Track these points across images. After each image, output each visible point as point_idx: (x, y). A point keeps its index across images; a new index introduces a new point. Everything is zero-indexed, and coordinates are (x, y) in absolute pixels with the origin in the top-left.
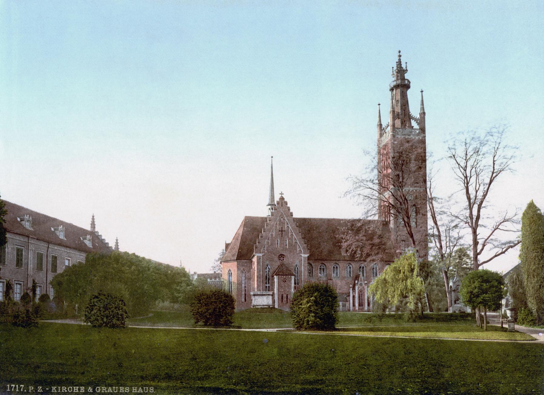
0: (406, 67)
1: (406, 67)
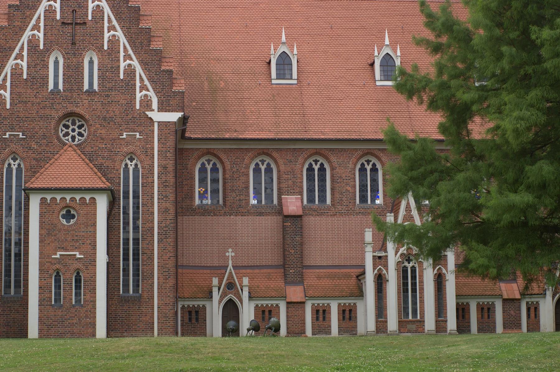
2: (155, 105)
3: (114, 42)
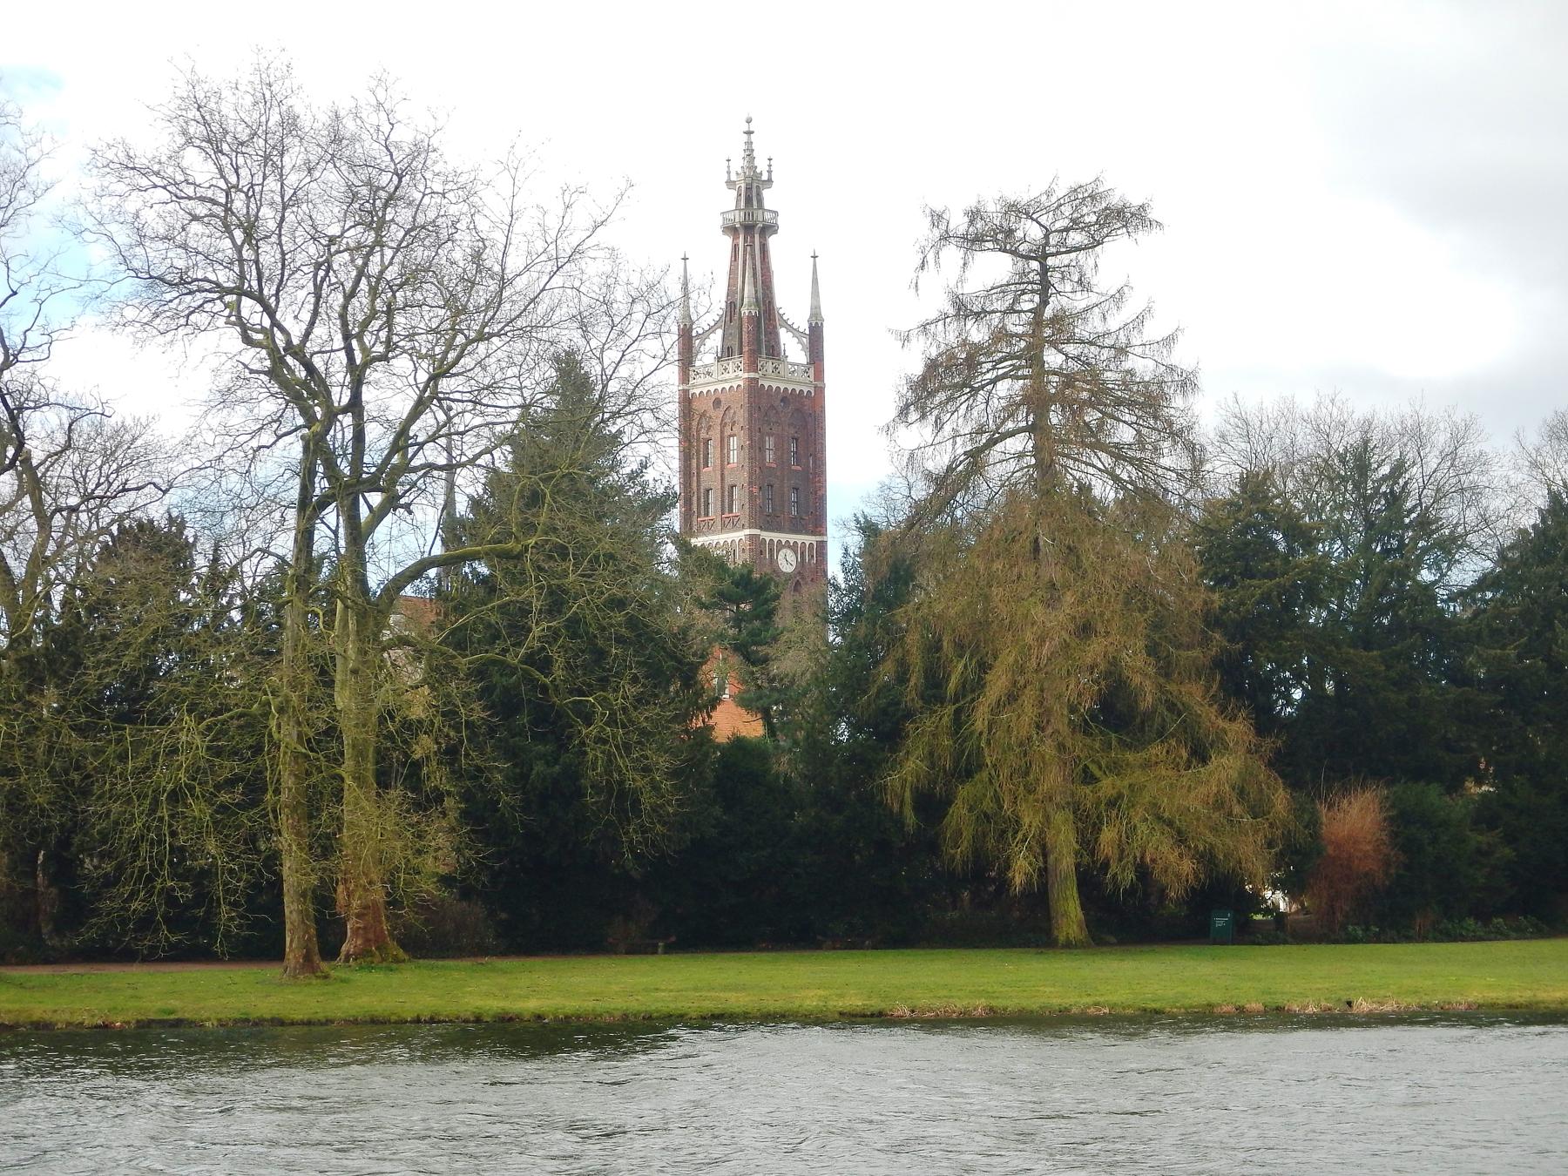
0: (770, 172)
1: (770, 172)
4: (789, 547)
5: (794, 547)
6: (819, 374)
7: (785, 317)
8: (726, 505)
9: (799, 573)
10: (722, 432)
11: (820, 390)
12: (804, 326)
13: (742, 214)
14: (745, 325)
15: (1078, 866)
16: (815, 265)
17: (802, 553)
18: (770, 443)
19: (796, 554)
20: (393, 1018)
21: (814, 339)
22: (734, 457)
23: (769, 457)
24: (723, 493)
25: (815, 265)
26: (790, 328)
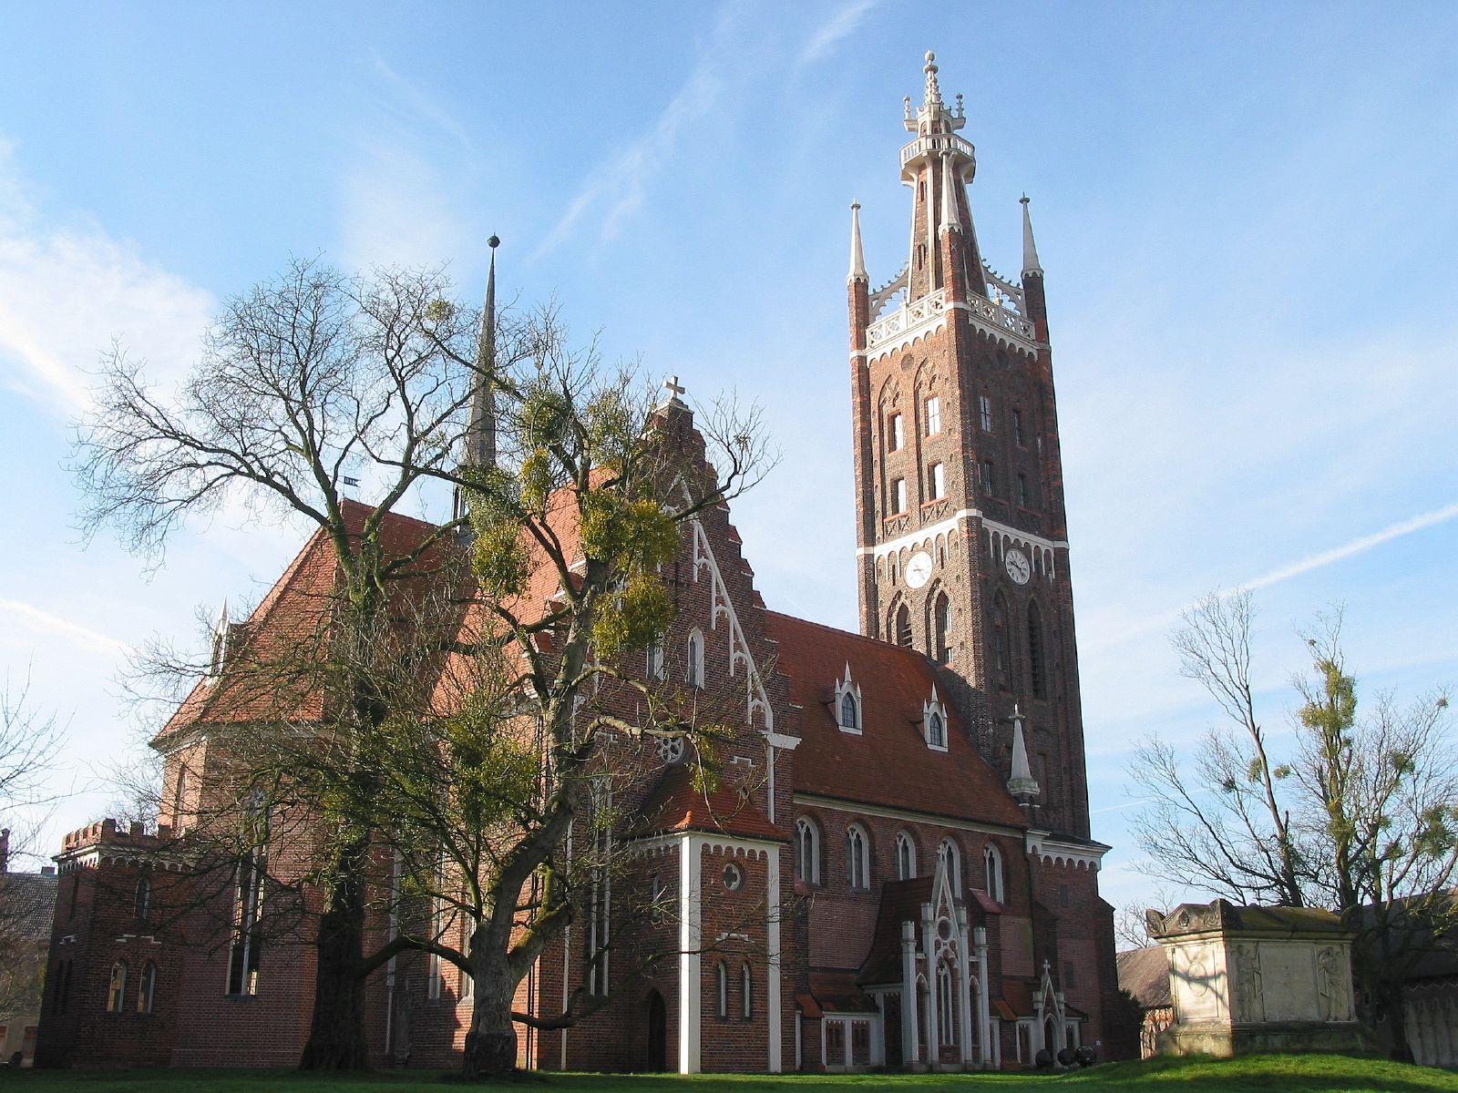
2: (769, 722)
3: (723, 621)
4: (1019, 548)
5: (1026, 550)
6: (1043, 334)
7: (997, 276)
8: (926, 487)
9: (1035, 588)
10: (916, 393)
11: (1046, 355)
12: (1017, 280)
13: (930, 141)
14: (945, 250)
15: (54, 945)
16: (1026, 215)
17: (1036, 562)
18: (985, 403)
19: (1029, 558)
20: (987, 821)
21: (1033, 287)
22: (935, 426)
23: (986, 425)
24: (920, 475)
25: (1026, 215)
26: (998, 283)
